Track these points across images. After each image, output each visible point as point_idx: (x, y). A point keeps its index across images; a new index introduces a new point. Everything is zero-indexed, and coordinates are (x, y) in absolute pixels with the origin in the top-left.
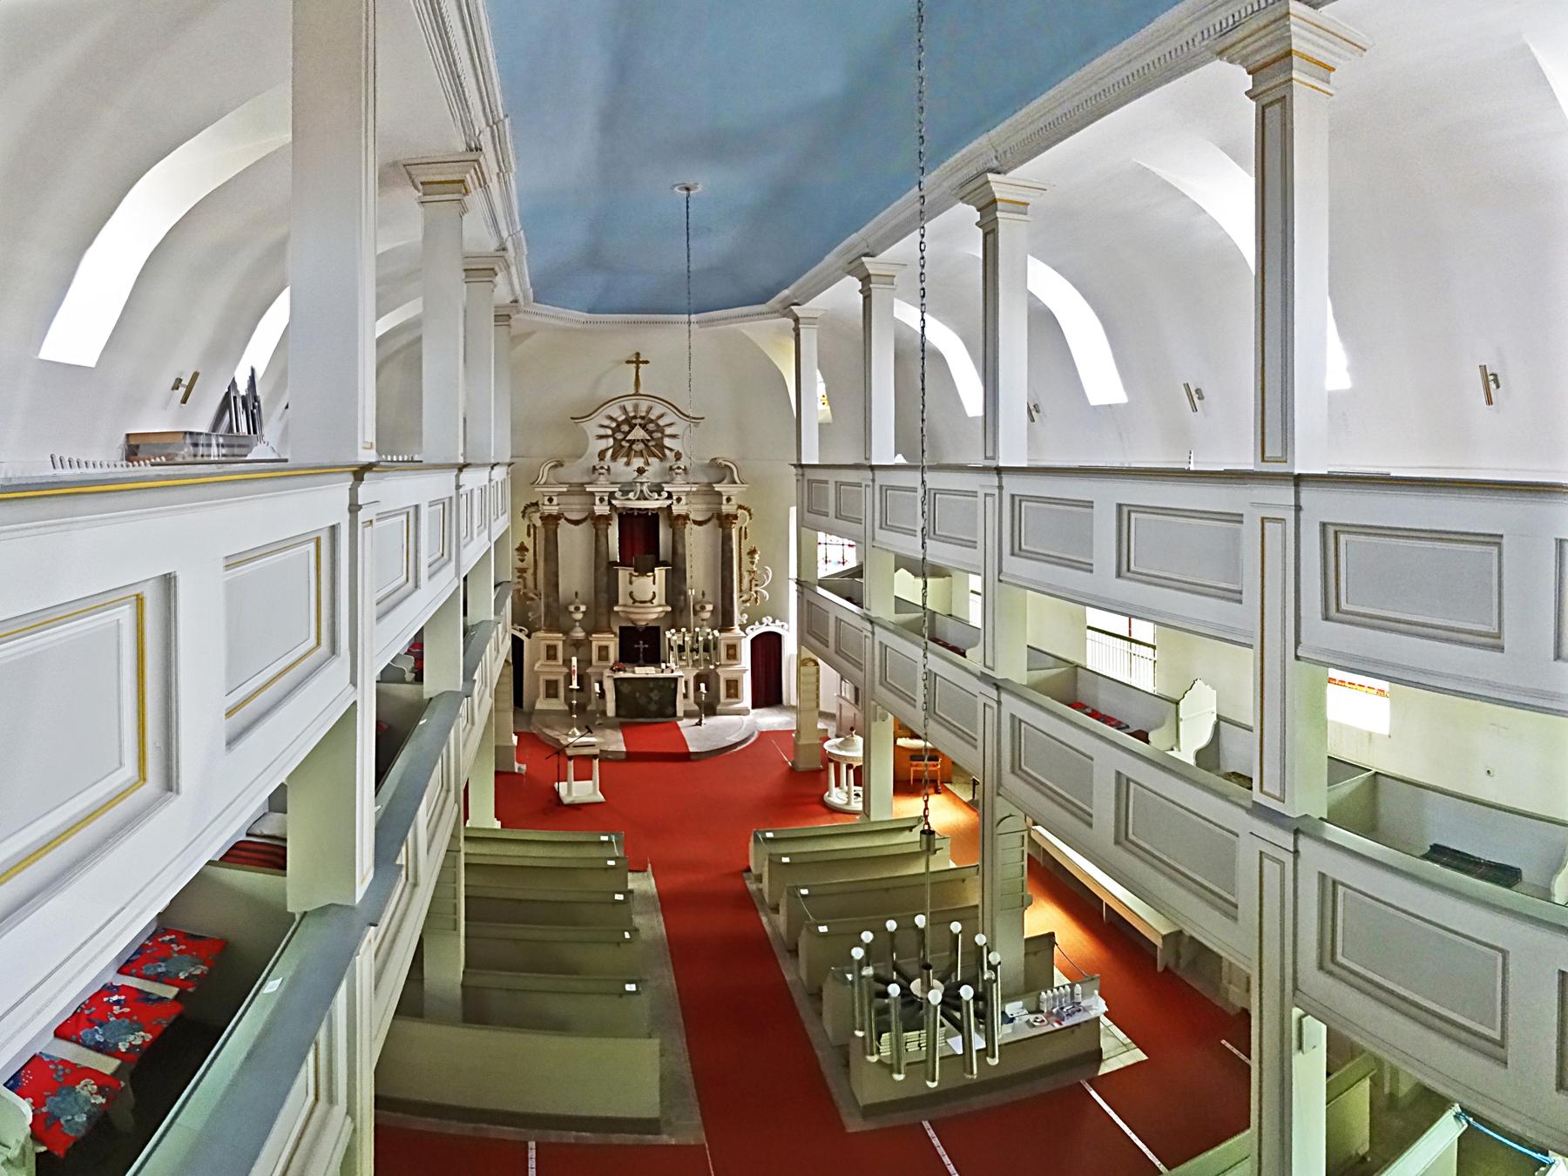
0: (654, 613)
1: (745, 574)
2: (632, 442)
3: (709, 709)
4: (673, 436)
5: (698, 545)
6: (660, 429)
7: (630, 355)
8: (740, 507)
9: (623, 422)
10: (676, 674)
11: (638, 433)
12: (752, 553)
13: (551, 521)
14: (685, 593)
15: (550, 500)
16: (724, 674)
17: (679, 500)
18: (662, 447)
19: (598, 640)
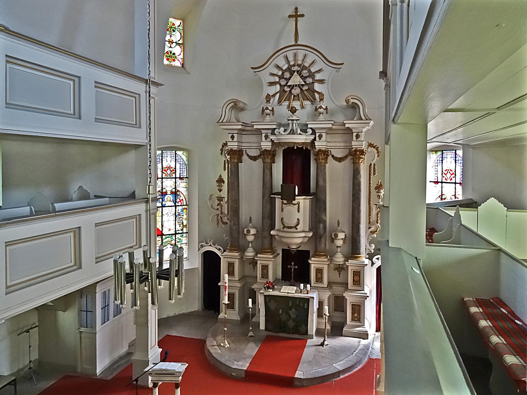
0: (298, 239)
1: (374, 208)
2: (292, 87)
3: (337, 330)
4: (321, 81)
5: (334, 177)
6: (312, 75)
7: (291, 12)
8: (370, 145)
9: (309, 71)
10: (310, 295)
11: (296, 80)
12: (379, 187)
13: (237, 155)
14: (325, 222)
15: (233, 137)
16: (350, 297)
17: (320, 137)
18: (312, 91)
19: (263, 259)
